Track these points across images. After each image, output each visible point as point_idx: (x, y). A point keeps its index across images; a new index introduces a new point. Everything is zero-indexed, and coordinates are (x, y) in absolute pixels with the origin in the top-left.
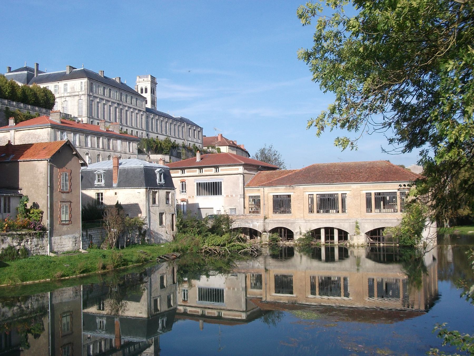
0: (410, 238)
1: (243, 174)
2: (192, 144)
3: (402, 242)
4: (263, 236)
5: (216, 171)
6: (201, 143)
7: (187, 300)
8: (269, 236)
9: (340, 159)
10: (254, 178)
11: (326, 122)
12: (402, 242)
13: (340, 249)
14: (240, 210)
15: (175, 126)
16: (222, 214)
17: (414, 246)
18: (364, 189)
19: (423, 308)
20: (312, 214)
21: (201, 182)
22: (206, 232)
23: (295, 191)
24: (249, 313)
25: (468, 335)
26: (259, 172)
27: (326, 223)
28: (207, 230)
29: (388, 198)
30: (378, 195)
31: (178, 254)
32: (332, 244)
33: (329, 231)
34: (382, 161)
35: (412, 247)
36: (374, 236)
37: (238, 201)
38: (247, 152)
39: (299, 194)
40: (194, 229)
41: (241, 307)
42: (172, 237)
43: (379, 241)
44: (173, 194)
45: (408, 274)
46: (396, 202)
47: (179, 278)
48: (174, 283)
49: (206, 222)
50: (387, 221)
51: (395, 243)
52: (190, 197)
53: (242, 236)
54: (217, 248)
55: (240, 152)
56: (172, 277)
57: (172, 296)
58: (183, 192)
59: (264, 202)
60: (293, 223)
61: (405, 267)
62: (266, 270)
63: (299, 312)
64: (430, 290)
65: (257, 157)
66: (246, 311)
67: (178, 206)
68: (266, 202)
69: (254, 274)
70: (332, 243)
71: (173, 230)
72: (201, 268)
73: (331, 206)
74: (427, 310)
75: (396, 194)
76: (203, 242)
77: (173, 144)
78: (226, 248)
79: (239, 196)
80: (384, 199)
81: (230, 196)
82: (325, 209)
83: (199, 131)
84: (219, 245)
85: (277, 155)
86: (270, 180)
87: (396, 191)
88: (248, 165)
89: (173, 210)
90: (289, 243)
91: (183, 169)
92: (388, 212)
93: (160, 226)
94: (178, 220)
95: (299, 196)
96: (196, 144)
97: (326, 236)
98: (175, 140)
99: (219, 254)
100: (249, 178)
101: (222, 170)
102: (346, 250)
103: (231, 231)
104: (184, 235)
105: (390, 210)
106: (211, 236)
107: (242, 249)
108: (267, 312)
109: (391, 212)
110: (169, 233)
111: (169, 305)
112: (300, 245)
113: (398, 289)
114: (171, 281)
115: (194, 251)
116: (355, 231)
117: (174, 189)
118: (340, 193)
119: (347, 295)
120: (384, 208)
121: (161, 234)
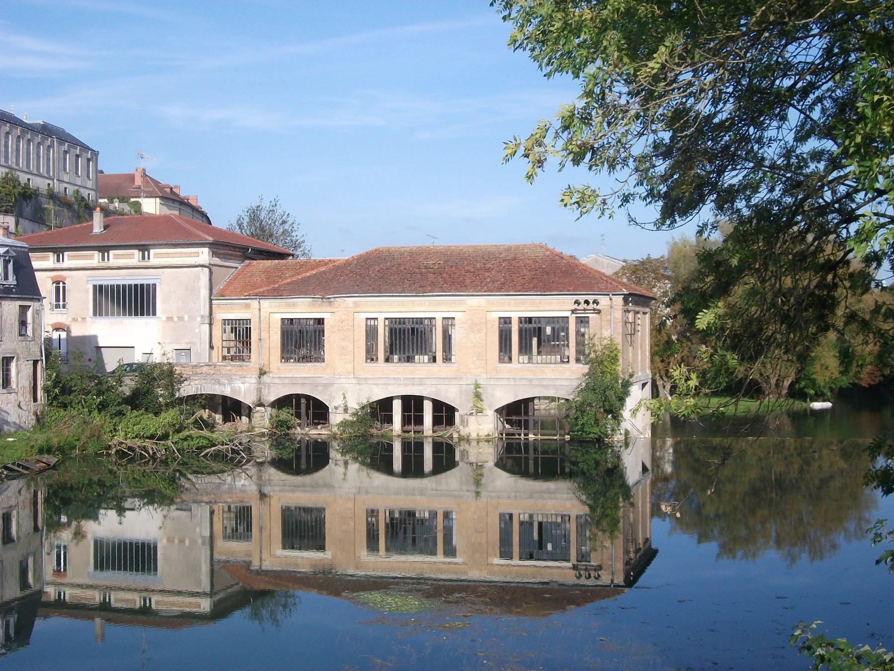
0: (595, 423)
1: (210, 267)
2: (71, 190)
3: (578, 431)
4: (256, 415)
5: (143, 258)
6: (94, 188)
7: (65, 570)
8: (271, 415)
9: (433, 237)
10: (235, 278)
11: (549, 148)
12: (578, 431)
13: (438, 447)
14: (201, 353)
15: (29, 145)
16: (157, 361)
17: (603, 440)
18: (494, 309)
19: (620, 579)
20: (372, 365)
21: (104, 283)
22: (119, 404)
23: (334, 310)
24: (217, 598)
25: (867, 648)
26: (247, 262)
27: (406, 385)
28: (120, 400)
29: (548, 330)
30: (526, 323)
31: (53, 460)
32: (417, 435)
33: (413, 405)
34: (536, 246)
35: (600, 443)
36: (514, 418)
37: (197, 331)
38: (204, 215)
39: (343, 317)
40: (89, 397)
41: (199, 583)
42: (34, 417)
43: (526, 428)
44: (38, 313)
45: (589, 502)
46: (568, 339)
47: (51, 517)
48: (36, 529)
49: (120, 381)
50: (545, 383)
51: (563, 432)
52: (75, 320)
53: (205, 414)
54: (148, 443)
55: (188, 214)
56: (32, 515)
57: (31, 561)
58: (57, 306)
59: (260, 334)
60: (327, 386)
61: (584, 488)
62: (263, 496)
63: (375, 597)
64: (635, 541)
65: (240, 226)
66: (212, 594)
67: (49, 341)
68: (264, 335)
69: (233, 506)
70: (419, 432)
71: (35, 400)
72: (104, 492)
73: (417, 345)
74: (630, 582)
75: (568, 322)
76: (112, 428)
77: (23, 188)
78: (169, 443)
79: (199, 319)
80: (539, 332)
81: (175, 319)
82: (404, 353)
83: (89, 160)
84: (152, 437)
85: (289, 223)
86: (275, 282)
87: (568, 314)
88: (223, 245)
89: (36, 350)
90: (318, 433)
91: (59, 251)
92: (549, 361)
93: (5, 391)
94: (50, 376)
95: (343, 322)
96: (82, 190)
97: (403, 417)
98: (29, 180)
99: (153, 457)
100: (224, 276)
101: (157, 256)
102: (451, 449)
103: (181, 400)
104: (62, 412)
105: (553, 357)
106: (132, 415)
107: (211, 447)
108: (263, 594)
109: (555, 363)
110: (24, 407)
111: (24, 584)
112: (344, 436)
113: (566, 537)
114: (28, 524)
115: (91, 450)
116: (471, 405)
117: (39, 300)
118: (439, 316)
119: (450, 551)
120: (539, 353)
121: (5, 408)
